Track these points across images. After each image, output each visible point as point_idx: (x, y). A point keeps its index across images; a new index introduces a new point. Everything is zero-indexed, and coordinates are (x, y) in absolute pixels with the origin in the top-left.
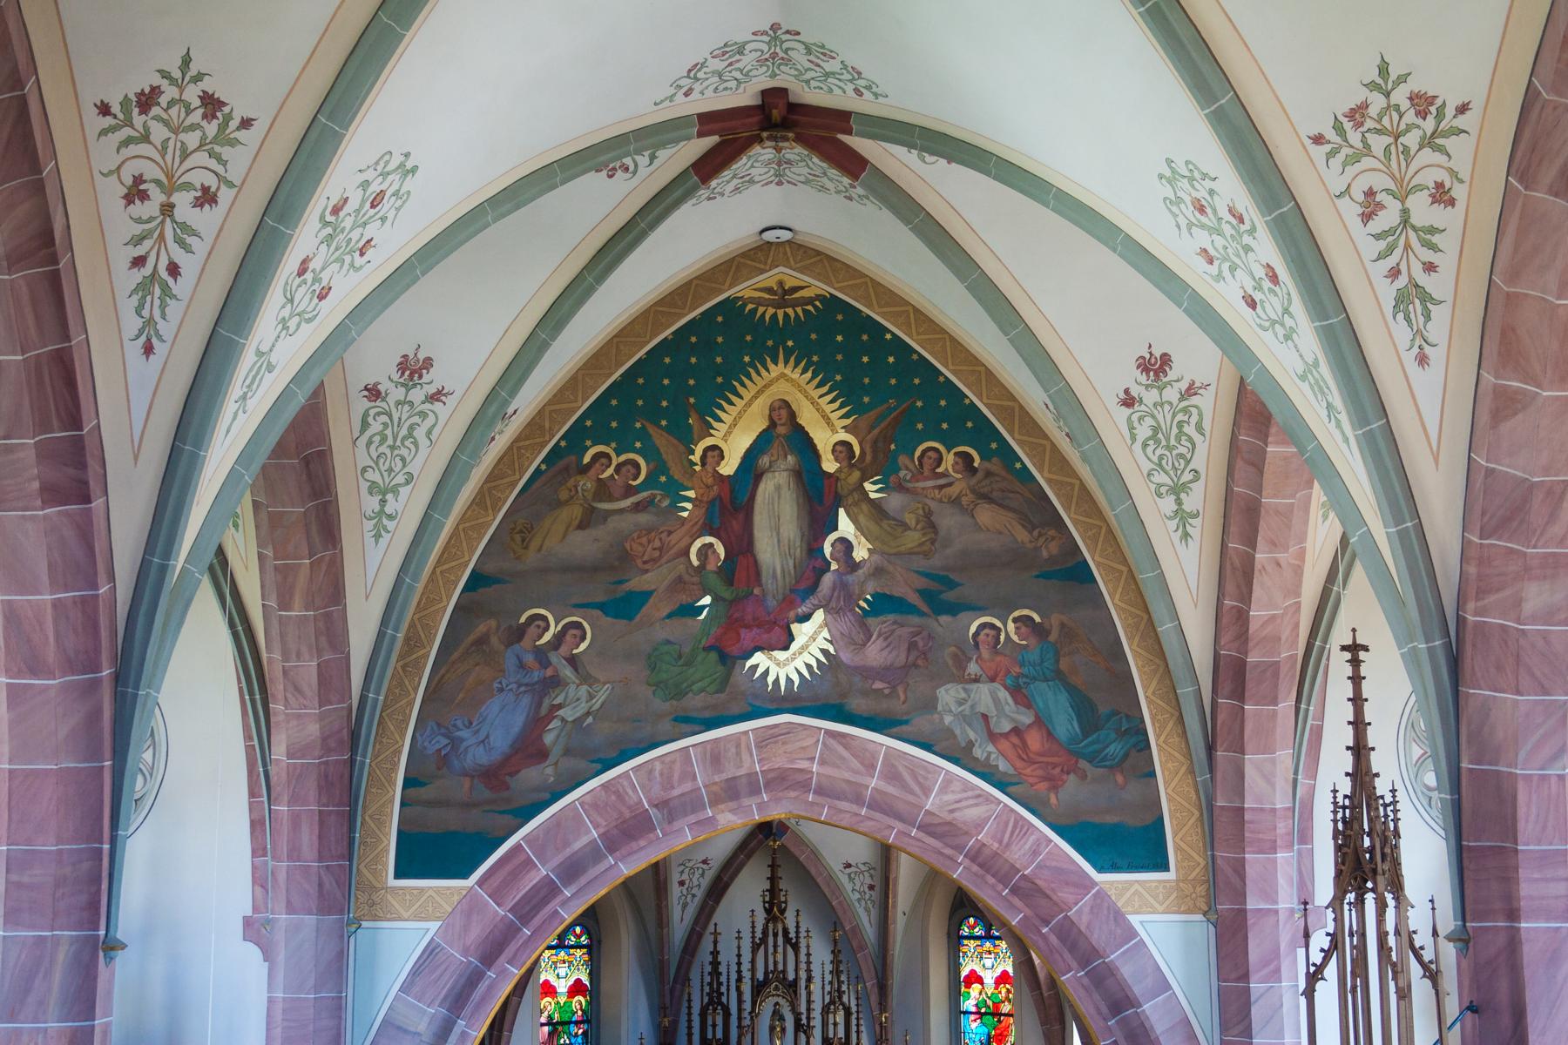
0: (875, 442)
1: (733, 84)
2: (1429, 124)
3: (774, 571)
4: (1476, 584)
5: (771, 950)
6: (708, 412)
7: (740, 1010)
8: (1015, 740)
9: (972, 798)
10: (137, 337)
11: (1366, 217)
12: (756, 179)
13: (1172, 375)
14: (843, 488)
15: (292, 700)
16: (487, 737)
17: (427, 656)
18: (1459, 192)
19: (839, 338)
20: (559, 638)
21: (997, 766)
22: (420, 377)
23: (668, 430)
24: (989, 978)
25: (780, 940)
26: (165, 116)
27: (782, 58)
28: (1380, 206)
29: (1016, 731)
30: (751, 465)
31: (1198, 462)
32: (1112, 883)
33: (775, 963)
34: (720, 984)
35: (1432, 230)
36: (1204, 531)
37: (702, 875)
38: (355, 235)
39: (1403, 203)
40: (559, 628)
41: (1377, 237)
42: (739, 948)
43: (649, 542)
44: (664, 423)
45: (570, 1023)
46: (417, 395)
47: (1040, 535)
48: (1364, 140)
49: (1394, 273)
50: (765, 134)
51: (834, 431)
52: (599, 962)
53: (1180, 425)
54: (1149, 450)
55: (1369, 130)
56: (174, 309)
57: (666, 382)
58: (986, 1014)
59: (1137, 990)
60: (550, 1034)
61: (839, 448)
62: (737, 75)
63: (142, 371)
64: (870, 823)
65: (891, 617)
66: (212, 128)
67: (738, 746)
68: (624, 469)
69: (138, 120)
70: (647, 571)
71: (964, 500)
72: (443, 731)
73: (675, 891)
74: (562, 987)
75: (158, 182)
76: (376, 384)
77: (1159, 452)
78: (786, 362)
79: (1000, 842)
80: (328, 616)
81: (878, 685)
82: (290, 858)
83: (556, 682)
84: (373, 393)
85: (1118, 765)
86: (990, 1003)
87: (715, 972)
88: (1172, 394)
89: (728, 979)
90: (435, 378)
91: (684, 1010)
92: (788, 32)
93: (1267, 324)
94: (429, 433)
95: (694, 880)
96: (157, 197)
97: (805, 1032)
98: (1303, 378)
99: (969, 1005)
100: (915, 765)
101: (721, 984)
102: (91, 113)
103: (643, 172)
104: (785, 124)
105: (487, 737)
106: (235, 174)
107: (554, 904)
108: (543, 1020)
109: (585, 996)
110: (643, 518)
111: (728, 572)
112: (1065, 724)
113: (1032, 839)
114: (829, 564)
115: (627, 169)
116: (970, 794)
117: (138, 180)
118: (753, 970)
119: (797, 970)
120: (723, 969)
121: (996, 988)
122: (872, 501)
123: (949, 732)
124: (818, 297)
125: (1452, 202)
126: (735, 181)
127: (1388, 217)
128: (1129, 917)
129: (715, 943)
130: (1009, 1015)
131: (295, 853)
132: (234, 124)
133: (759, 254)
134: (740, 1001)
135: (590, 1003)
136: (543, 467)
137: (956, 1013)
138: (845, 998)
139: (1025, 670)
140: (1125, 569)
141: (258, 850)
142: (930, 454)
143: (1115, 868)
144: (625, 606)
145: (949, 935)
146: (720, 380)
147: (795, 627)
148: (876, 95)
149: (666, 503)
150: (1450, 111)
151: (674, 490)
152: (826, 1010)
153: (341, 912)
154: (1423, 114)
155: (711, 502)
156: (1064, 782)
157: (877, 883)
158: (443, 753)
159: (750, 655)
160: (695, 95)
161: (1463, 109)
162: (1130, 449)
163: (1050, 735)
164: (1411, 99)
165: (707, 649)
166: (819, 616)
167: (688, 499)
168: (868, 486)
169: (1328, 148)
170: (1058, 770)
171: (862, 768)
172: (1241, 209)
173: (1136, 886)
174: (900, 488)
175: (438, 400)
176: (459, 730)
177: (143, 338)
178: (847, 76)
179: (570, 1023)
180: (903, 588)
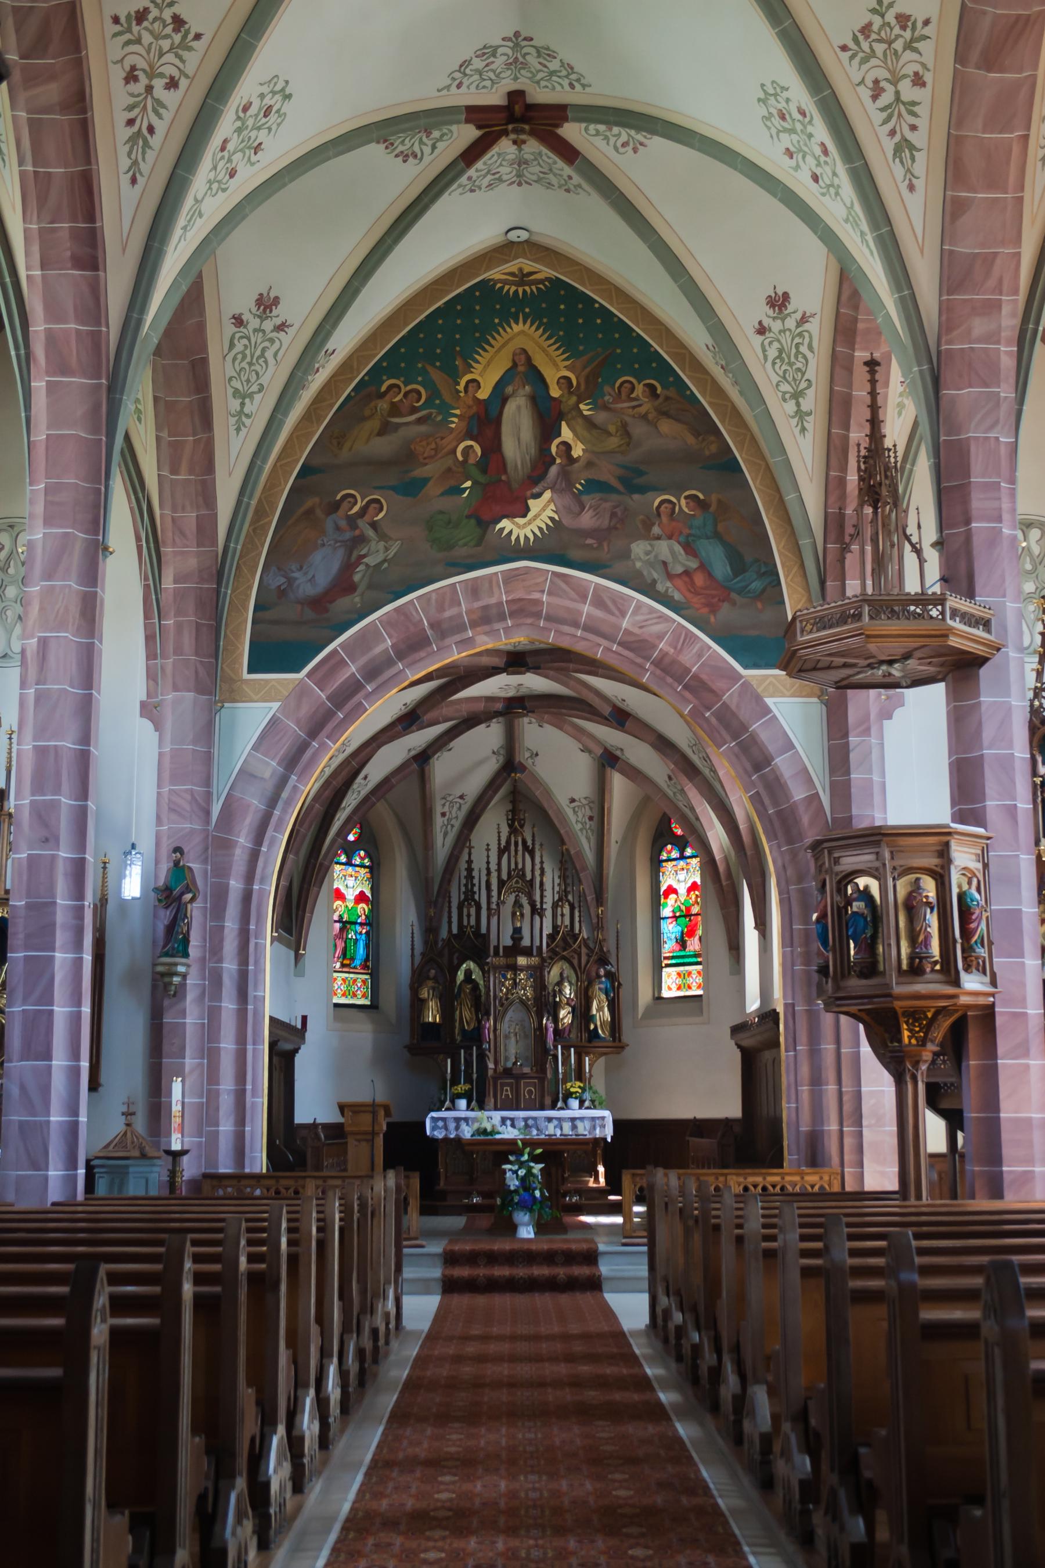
0: (587, 378)
1: (488, 83)
2: (908, 35)
3: (516, 466)
4: (947, 325)
5: (513, 853)
6: (469, 361)
7: (489, 903)
8: (687, 579)
10: (128, 171)
11: (875, 98)
12: (505, 177)
13: (790, 308)
14: (564, 408)
15: (177, 540)
16: (314, 576)
17: (271, 522)
18: (928, 77)
19: (562, 307)
20: (364, 510)
22: (271, 311)
23: (440, 368)
25: (520, 847)
26: (150, 27)
27: (522, 63)
28: (883, 90)
29: (687, 573)
30: (500, 397)
31: (810, 374)
33: (516, 864)
34: (473, 885)
35: (914, 104)
36: (816, 424)
37: (460, 808)
38: (253, 134)
39: (896, 87)
40: (364, 502)
41: (882, 110)
42: (488, 857)
43: (428, 444)
44: (438, 364)
45: (355, 923)
46: (268, 325)
47: (704, 440)
48: (871, 47)
49: (892, 133)
50: (510, 127)
51: (558, 370)
53: (797, 345)
54: (777, 366)
55: (873, 41)
56: (150, 155)
57: (439, 336)
58: (680, 916)
59: (772, 748)
61: (562, 381)
62: (492, 75)
63: (130, 195)
64: (583, 643)
65: (598, 496)
66: (177, 38)
67: (491, 582)
68: (410, 396)
69: (136, 29)
70: (426, 464)
71: (650, 417)
73: (439, 821)
74: (351, 895)
75: (144, 70)
76: (241, 314)
77: (784, 367)
78: (525, 323)
79: (675, 648)
80: (204, 483)
81: (589, 541)
82: (175, 653)
83: (361, 540)
84: (238, 321)
85: (760, 596)
86: (684, 908)
87: (470, 877)
88: (790, 323)
90: (281, 313)
91: (446, 915)
92: (525, 39)
93: (825, 190)
94: (275, 355)
96: (143, 80)
98: (847, 221)
99: (666, 912)
100: (616, 597)
102: (108, 21)
103: (427, 159)
104: (524, 119)
105: (314, 576)
106: (190, 69)
107: (359, 697)
108: (336, 918)
110: (423, 429)
111: (483, 465)
112: (721, 568)
114: (555, 459)
115: (416, 156)
117: (133, 68)
118: (499, 870)
119: (533, 871)
120: (475, 873)
121: (688, 895)
122: (585, 417)
123: (639, 574)
124: (547, 279)
125: (924, 85)
126: (489, 177)
127: (887, 98)
128: (766, 700)
129: (470, 854)
130: (697, 914)
131: (178, 650)
132: (191, 36)
133: (505, 250)
134: (489, 897)
135: (371, 911)
136: (353, 394)
137: (657, 919)
138: (570, 897)
139: (693, 532)
140: (763, 463)
141: (151, 655)
142: (626, 385)
143: (756, 666)
144: (412, 488)
145: (652, 859)
146: (477, 335)
147: (531, 502)
148: (584, 86)
149: (439, 418)
150: (919, 25)
151: (445, 409)
152: (555, 906)
153: (210, 694)
154: (904, 28)
155: (471, 418)
157: (595, 814)
159: (499, 521)
160: (464, 89)
161: (927, 22)
162: (764, 367)
163: (710, 575)
164: (896, 18)
165: (468, 517)
166: (548, 495)
167: (455, 416)
168: (582, 406)
169: (850, 53)
170: (716, 600)
171: (576, 597)
172: (804, 106)
173: (771, 679)
174: (606, 408)
175: (283, 330)
176: (293, 572)
177: (131, 173)
178: (564, 73)
179: (355, 923)
180: (606, 473)
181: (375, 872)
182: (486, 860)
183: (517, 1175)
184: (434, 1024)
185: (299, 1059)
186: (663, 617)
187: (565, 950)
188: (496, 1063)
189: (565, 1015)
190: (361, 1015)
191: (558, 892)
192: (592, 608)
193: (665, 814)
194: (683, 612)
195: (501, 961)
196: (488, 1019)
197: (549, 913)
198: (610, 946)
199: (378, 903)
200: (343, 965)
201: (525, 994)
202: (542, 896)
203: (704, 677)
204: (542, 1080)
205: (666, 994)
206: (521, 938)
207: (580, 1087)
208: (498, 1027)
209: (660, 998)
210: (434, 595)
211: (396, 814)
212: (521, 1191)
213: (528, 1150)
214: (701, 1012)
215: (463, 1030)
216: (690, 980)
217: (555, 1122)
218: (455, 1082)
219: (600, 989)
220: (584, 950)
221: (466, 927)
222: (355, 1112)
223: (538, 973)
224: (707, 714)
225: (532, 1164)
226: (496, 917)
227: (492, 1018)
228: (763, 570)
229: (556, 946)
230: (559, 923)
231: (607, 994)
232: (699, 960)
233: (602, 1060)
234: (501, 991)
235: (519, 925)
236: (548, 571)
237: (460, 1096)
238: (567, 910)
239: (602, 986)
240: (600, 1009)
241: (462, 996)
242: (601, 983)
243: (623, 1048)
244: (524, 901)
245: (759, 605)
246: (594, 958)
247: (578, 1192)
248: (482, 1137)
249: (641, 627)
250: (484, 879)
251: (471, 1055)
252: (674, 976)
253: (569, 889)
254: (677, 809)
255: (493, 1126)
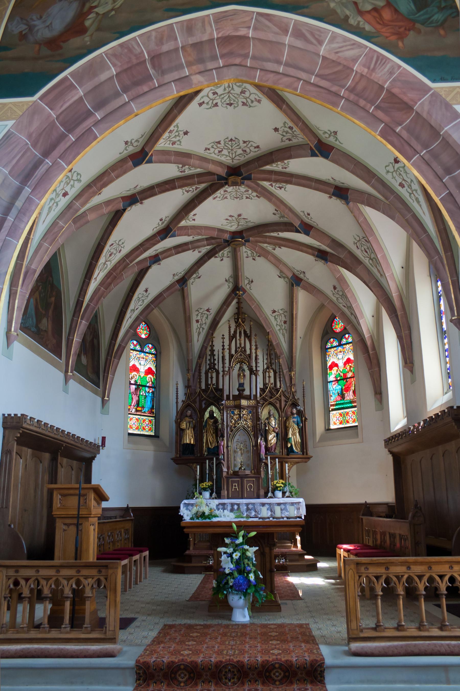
5: (238, 337)
8: (376, 14)
9: (350, 45)
16: (51, 23)
21: (364, 28)
24: (341, 364)
32: (442, 88)
33: (240, 344)
34: (214, 360)
37: (207, 318)
42: (223, 342)
45: (145, 386)
52: (160, 361)
58: (340, 380)
60: (135, 389)
67: (203, 22)
72: (25, 22)
73: (195, 326)
74: (142, 369)
79: (369, 68)
87: (212, 355)
89: (218, 357)
95: (203, 320)
97: (254, 374)
99: (331, 378)
100: (313, 31)
101: (215, 360)
105: (51, 23)
108: (132, 382)
109: (153, 376)
113: (388, 66)
116: (348, 43)
118: (230, 349)
119: (251, 349)
120: (216, 353)
121: (344, 367)
123: (334, 12)
130: (351, 378)
137: (326, 382)
143: (443, 80)
152: (264, 372)
156: (407, 35)
157: (288, 320)
158: (24, 33)
163: (396, 11)
179: (145, 386)
181: (158, 356)
182: (222, 344)
183: (232, 558)
184: (190, 444)
185: (95, 465)
186: (355, 44)
187: (271, 398)
188: (228, 468)
189: (272, 438)
190: (147, 440)
191: (267, 364)
192: (292, 39)
193: (333, 314)
194: (374, 40)
195: (231, 403)
196: (223, 440)
197: (260, 373)
198: (299, 395)
199: (160, 373)
200: (137, 411)
201: (246, 424)
202: (256, 363)
203: (396, 91)
204: (258, 478)
205: (332, 427)
206: (244, 390)
207: (282, 483)
208: (230, 444)
209: (329, 429)
210: (154, 34)
211: (170, 324)
212: (236, 574)
213: (242, 533)
214: (357, 435)
215: (209, 448)
216: (347, 418)
217: (267, 506)
218: (202, 480)
219: (293, 421)
220: (283, 398)
221: (210, 385)
222: (64, 495)
223: (254, 411)
224: (398, 130)
225: (246, 547)
226: (228, 376)
227: (225, 439)
228: (443, 5)
229: (266, 396)
230: (267, 382)
231: (298, 425)
232: (355, 404)
233: (295, 467)
234: (231, 422)
235: (242, 382)
236: (254, 12)
237: (205, 489)
238: (272, 374)
239: (295, 420)
240: (294, 434)
241: (208, 427)
242: (294, 418)
243: (309, 458)
244: (245, 367)
245: (442, 32)
246: (290, 403)
247: (284, 555)
248: (200, 520)
249: (337, 53)
250: (221, 355)
251: (213, 463)
252: (338, 415)
253: (273, 361)
254: (339, 309)
255: (211, 509)
